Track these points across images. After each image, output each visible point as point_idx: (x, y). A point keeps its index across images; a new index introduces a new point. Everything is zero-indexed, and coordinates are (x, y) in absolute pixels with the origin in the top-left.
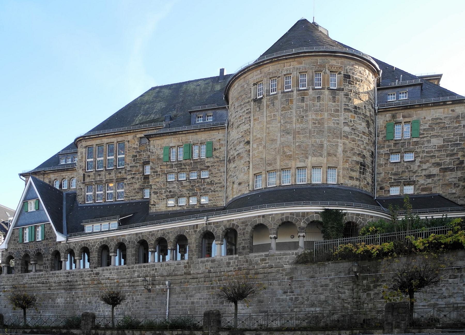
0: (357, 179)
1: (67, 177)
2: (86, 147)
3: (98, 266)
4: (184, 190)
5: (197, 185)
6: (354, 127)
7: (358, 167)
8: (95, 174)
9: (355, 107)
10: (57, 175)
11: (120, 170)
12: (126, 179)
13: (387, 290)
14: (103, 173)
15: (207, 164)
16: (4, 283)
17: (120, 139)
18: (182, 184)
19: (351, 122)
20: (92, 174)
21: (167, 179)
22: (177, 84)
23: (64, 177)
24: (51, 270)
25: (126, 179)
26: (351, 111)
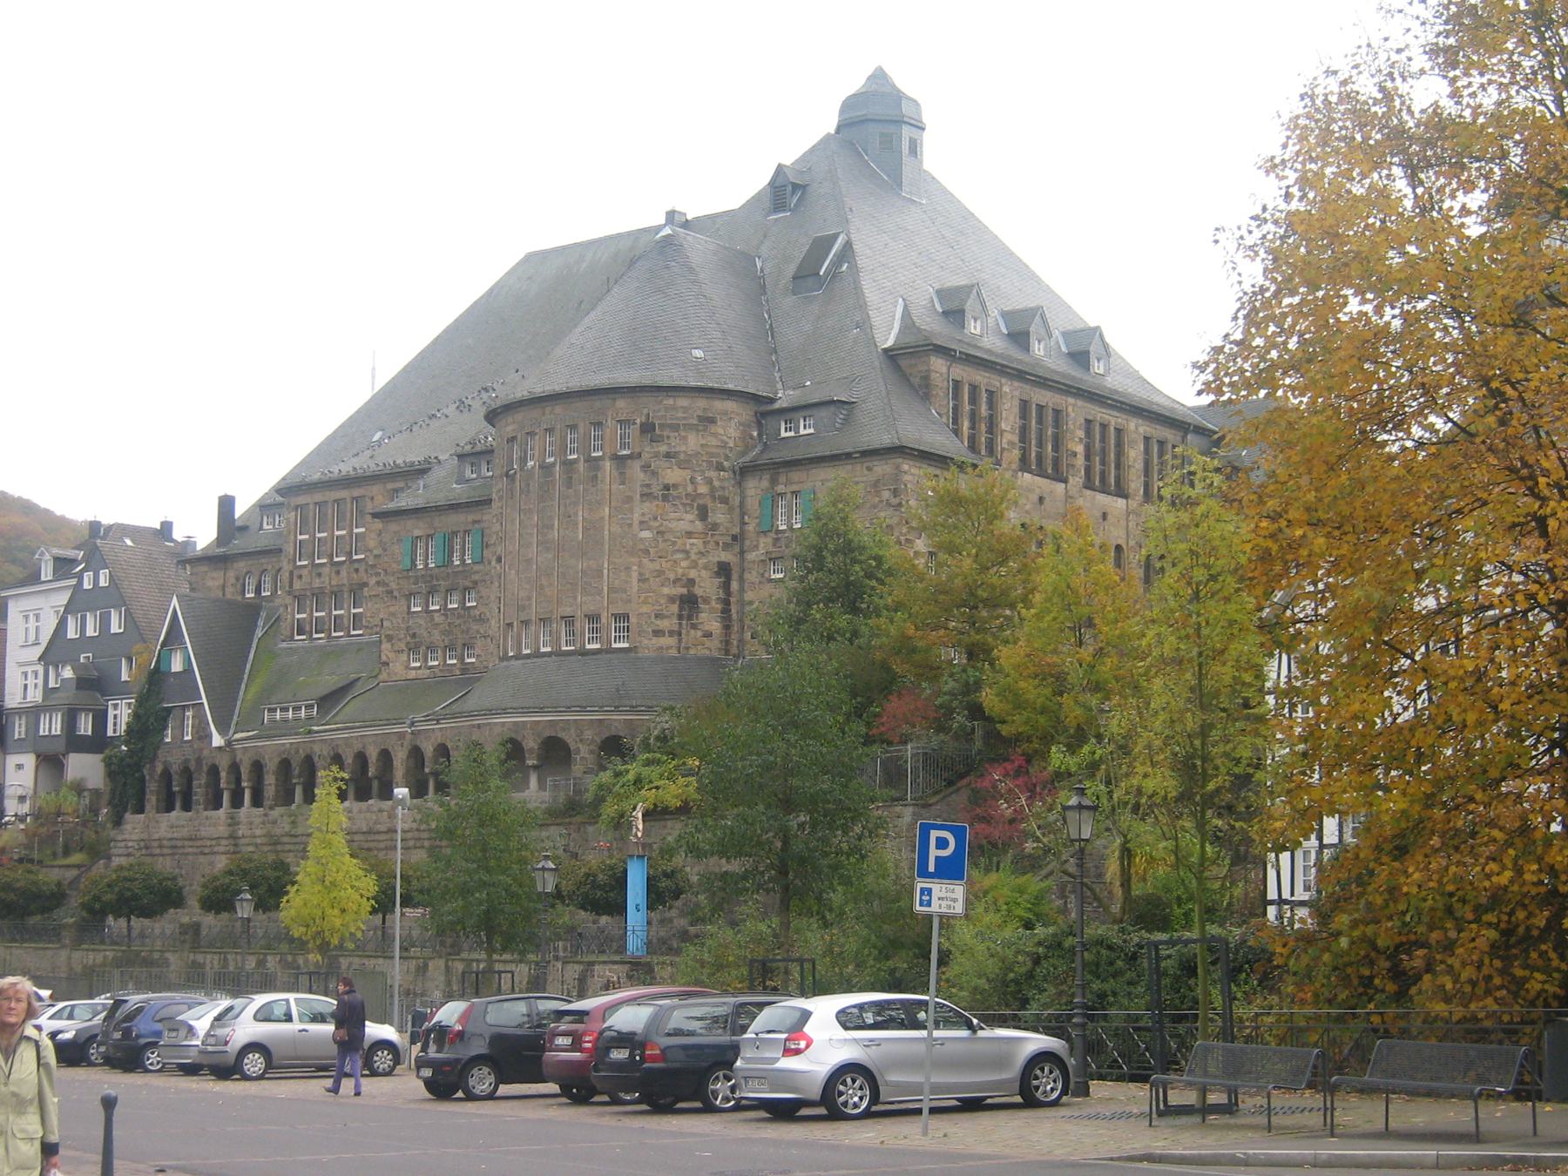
0: (671, 633)
1: (270, 567)
2: (296, 508)
3: (276, 805)
4: (436, 632)
5: (458, 622)
6: (662, 529)
7: (675, 608)
8: (310, 572)
9: (667, 487)
10: (250, 562)
11: (356, 566)
12: (365, 584)
13: (1391, 1011)
14: (326, 570)
15: (476, 577)
16: (127, 837)
17: (356, 492)
18: (432, 619)
19: (656, 519)
20: (305, 572)
21: (409, 608)
22: (564, 248)
23: (265, 567)
24: (206, 810)
25: (365, 584)
26: (656, 498)
